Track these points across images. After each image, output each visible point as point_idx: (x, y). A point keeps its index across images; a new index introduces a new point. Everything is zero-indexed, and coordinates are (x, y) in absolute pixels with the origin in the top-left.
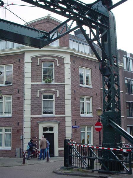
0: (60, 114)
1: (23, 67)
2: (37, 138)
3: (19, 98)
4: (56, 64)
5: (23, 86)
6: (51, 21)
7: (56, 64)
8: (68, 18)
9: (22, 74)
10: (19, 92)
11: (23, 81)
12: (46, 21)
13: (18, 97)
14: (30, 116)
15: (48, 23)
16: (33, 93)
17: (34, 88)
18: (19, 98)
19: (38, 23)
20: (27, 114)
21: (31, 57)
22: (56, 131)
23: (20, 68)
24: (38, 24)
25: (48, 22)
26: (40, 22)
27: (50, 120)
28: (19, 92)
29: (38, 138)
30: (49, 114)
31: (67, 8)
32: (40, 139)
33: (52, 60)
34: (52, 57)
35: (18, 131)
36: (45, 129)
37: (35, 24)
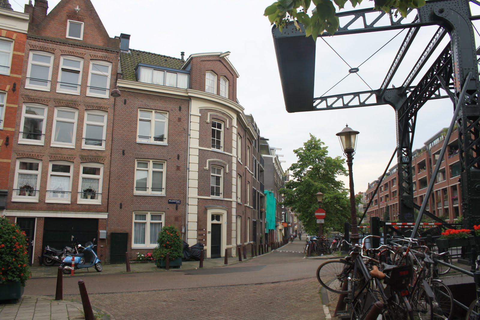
0: (454, 162)
1: (188, 121)
2: (204, 230)
3: (178, 168)
4: (225, 125)
5: (186, 149)
6: (223, 61)
7: (225, 125)
8: (468, 6)
9: (186, 132)
10: (178, 158)
11: (186, 142)
12: (218, 59)
13: (177, 166)
14: (196, 195)
15: (219, 63)
16: (201, 163)
17: (202, 155)
18: (178, 168)
19: (208, 59)
20: (193, 193)
21: (199, 108)
22: (224, 221)
23: (182, 120)
24: (207, 61)
25: (220, 61)
26: (211, 59)
27: (219, 205)
28: (178, 158)
29: (206, 230)
30: (216, 195)
31: (416, 5)
32: (209, 232)
33: (223, 120)
34: (223, 114)
35: (177, 219)
36: (213, 217)
37: (206, 59)
